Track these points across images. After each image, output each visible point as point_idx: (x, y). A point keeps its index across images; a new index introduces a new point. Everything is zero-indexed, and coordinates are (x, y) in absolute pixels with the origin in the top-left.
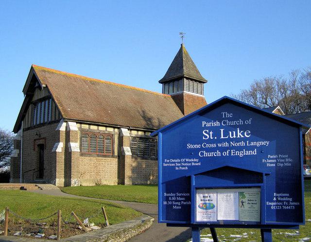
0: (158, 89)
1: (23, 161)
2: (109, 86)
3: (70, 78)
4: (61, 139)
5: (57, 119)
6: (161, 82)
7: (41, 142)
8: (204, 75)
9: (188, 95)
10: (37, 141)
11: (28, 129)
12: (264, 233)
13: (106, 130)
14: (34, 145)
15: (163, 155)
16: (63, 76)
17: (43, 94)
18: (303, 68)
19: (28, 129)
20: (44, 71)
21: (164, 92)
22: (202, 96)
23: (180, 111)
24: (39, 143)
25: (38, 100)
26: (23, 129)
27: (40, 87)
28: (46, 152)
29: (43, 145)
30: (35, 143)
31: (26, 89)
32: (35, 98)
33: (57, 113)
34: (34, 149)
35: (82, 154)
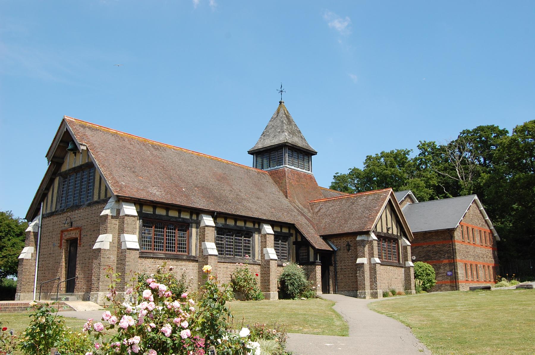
0: (249, 161)
1: (40, 265)
2: (180, 153)
3: (122, 138)
4: (109, 229)
5: (103, 196)
6: (251, 153)
7: (73, 235)
8: (313, 147)
9: (292, 171)
10: (66, 233)
11: (52, 214)
12: (37, 231)
13: (179, 217)
14: (61, 240)
15: (38, 234)
16: (113, 135)
17: (79, 161)
18: (532, 119)
19: (52, 214)
20: (84, 127)
21: (256, 166)
22: (310, 172)
23: (281, 193)
24: (68, 237)
25: (70, 170)
26: (43, 215)
27: (75, 150)
28: (80, 250)
29: (76, 239)
30: (61, 236)
31: (52, 155)
32: (65, 167)
33: (103, 188)
34: (60, 246)
35: (143, 256)
